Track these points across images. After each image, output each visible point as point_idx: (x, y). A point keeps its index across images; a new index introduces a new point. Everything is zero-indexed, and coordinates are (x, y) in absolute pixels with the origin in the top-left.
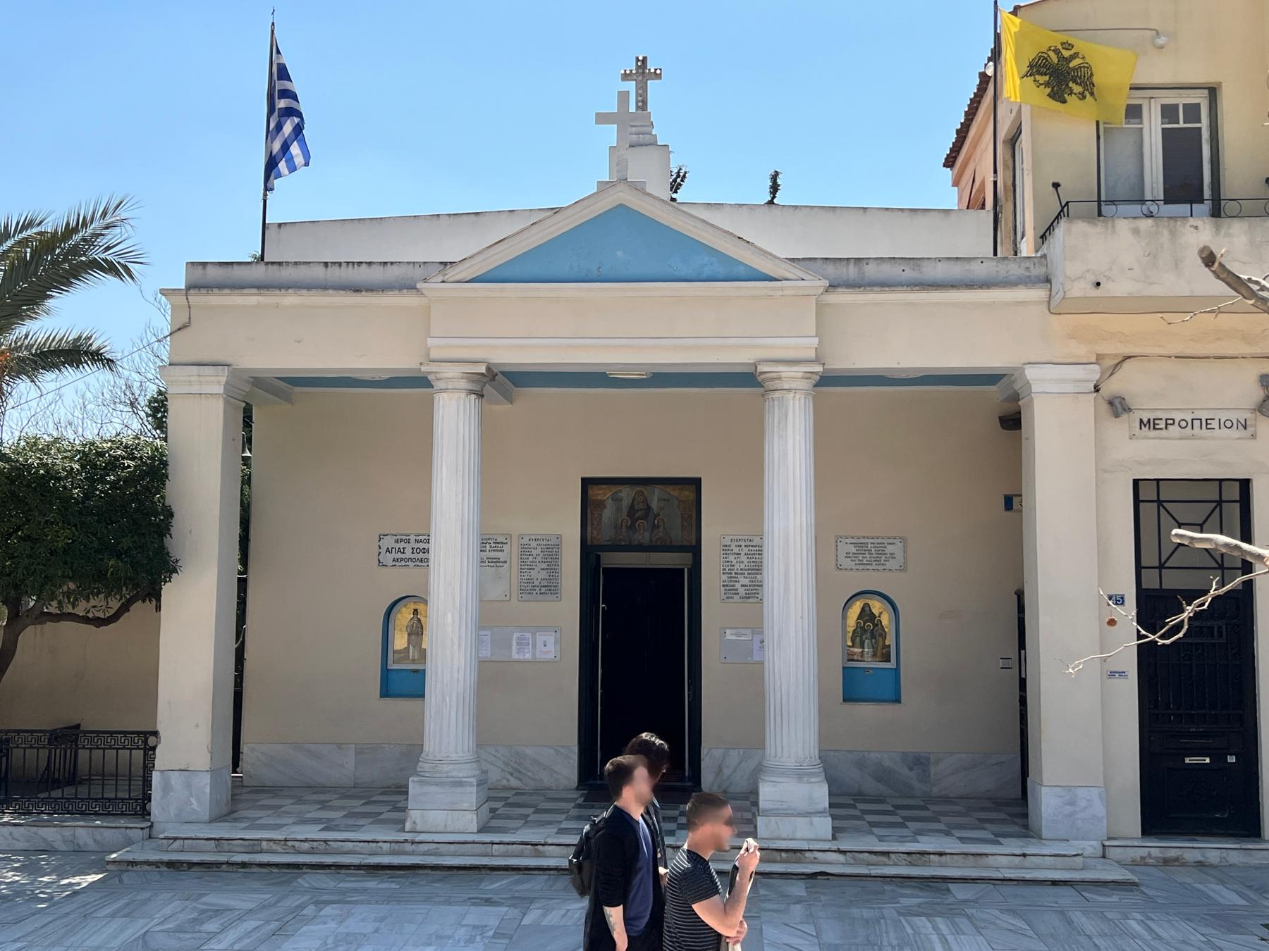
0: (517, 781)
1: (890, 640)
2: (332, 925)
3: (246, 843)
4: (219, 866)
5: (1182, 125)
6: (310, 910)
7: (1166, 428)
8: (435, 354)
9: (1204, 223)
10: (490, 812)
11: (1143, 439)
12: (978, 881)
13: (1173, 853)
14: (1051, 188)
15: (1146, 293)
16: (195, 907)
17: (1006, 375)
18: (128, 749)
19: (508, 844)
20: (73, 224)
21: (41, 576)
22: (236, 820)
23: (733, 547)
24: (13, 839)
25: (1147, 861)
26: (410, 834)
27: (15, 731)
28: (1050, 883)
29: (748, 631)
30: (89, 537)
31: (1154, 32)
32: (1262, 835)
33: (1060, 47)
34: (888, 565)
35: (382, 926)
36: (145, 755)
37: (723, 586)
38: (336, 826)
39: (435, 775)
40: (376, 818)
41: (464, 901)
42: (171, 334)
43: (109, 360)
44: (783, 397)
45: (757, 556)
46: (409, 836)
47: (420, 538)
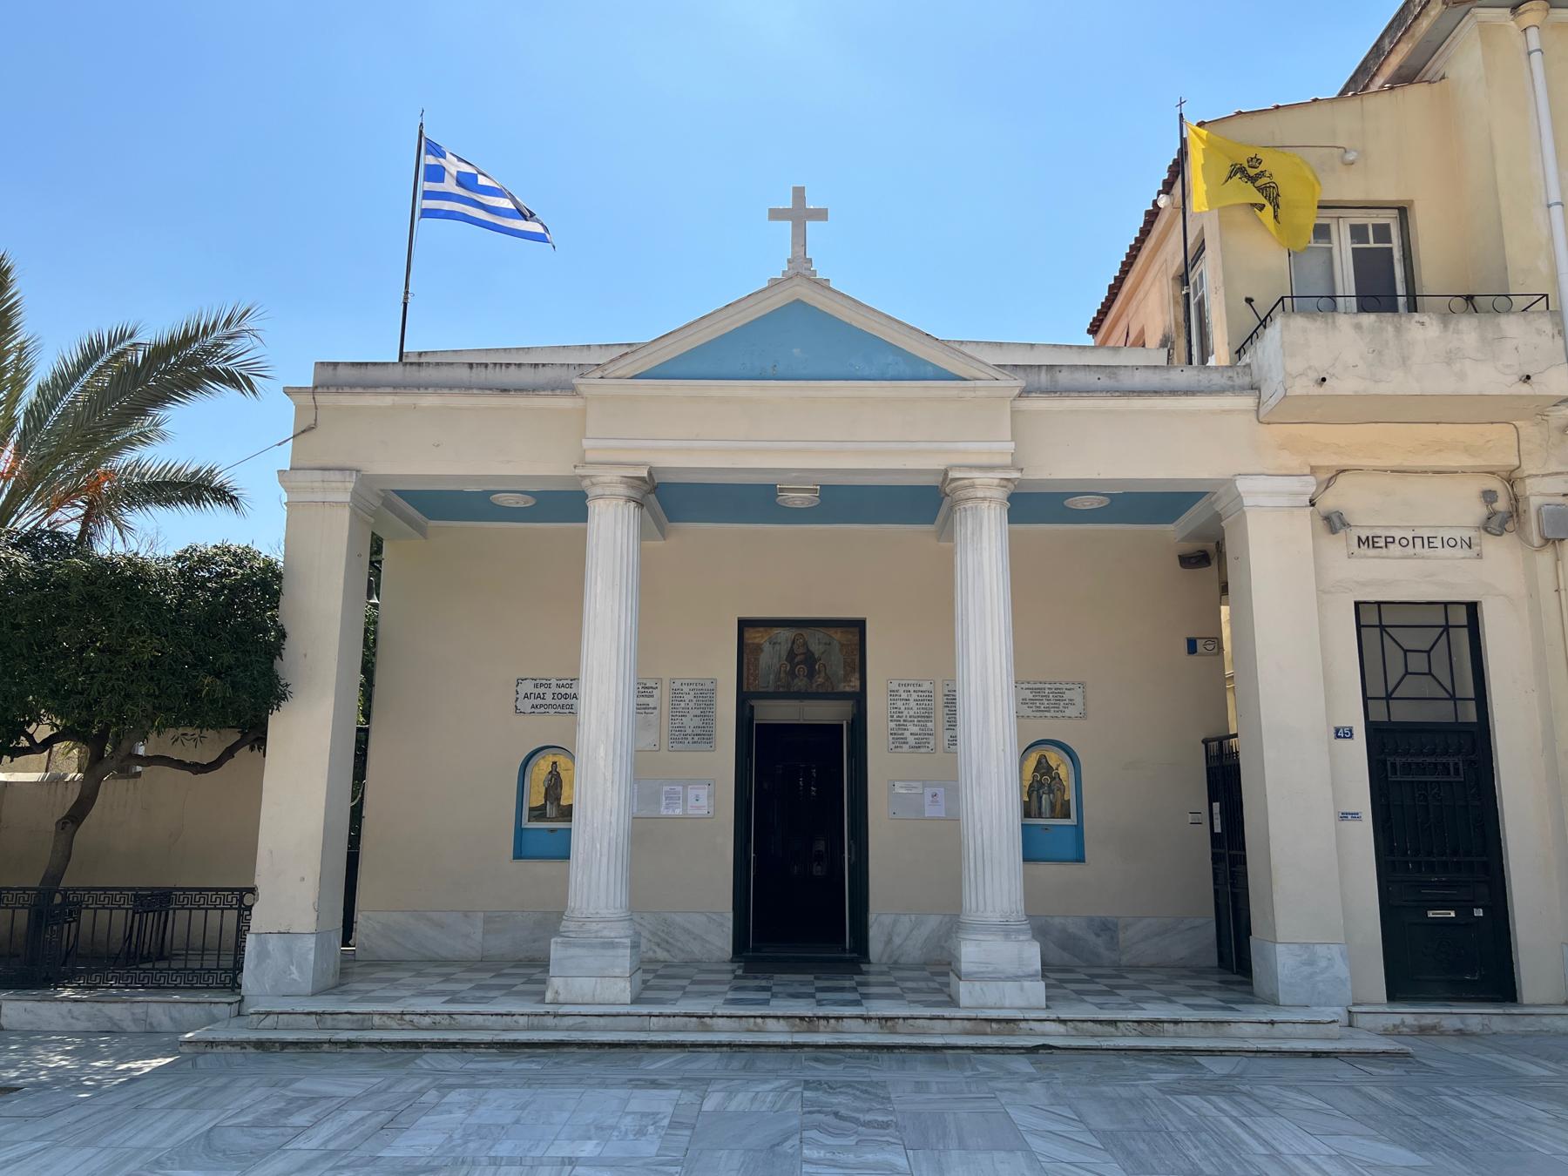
0: (665, 953)
1: (1070, 795)
2: (459, 1115)
3: (355, 1017)
4: (319, 1045)
5: (1372, 245)
6: (431, 1096)
7: (1386, 546)
8: (590, 457)
9: (1431, 319)
10: (643, 983)
11: (1362, 558)
12: (1226, 1053)
13: (1428, 1021)
14: (1244, 302)
15: (1374, 392)
16: (283, 1095)
17: (1205, 493)
18: (219, 909)
19: (669, 1016)
20: (191, 332)
21: (120, 693)
22: (343, 993)
23: (901, 692)
24: (72, 1018)
25: (1400, 1030)
26: (551, 1006)
27: (84, 889)
28: (1310, 1055)
29: (919, 784)
30: (182, 650)
31: (1343, 150)
32: (1518, 999)
33: (1246, 165)
34: (1068, 713)
35: (524, 1115)
36: (240, 915)
37: (891, 734)
38: (463, 998)
39: (581, 935)
40: (509, 990)
41: (625, 1084)
42: (294, 437)
43: (232, 497)
44: (976, 507)
45: (927, 703)
46: (550, 1009)
47: (561, 682)
